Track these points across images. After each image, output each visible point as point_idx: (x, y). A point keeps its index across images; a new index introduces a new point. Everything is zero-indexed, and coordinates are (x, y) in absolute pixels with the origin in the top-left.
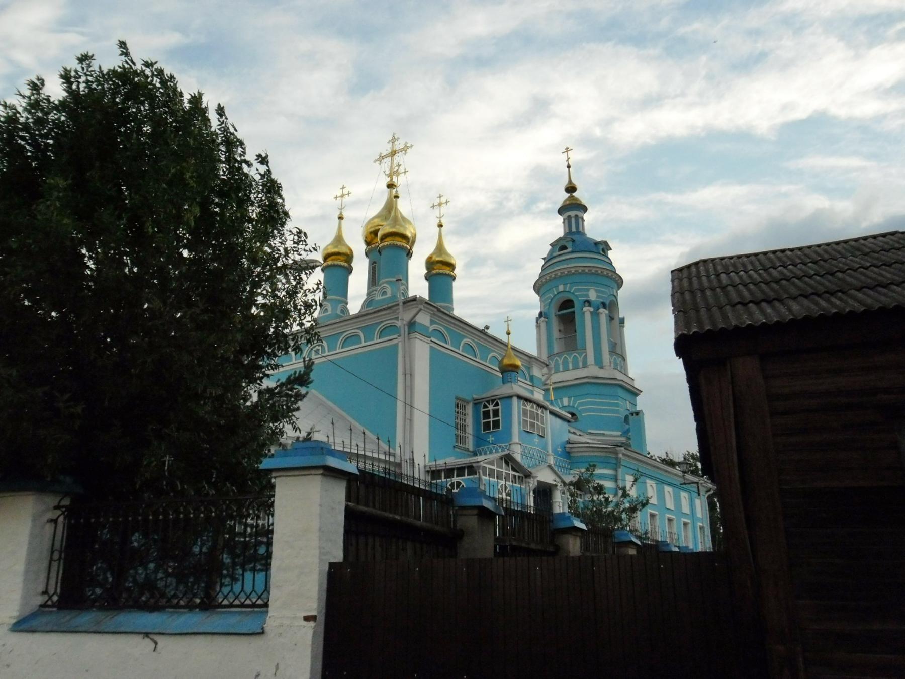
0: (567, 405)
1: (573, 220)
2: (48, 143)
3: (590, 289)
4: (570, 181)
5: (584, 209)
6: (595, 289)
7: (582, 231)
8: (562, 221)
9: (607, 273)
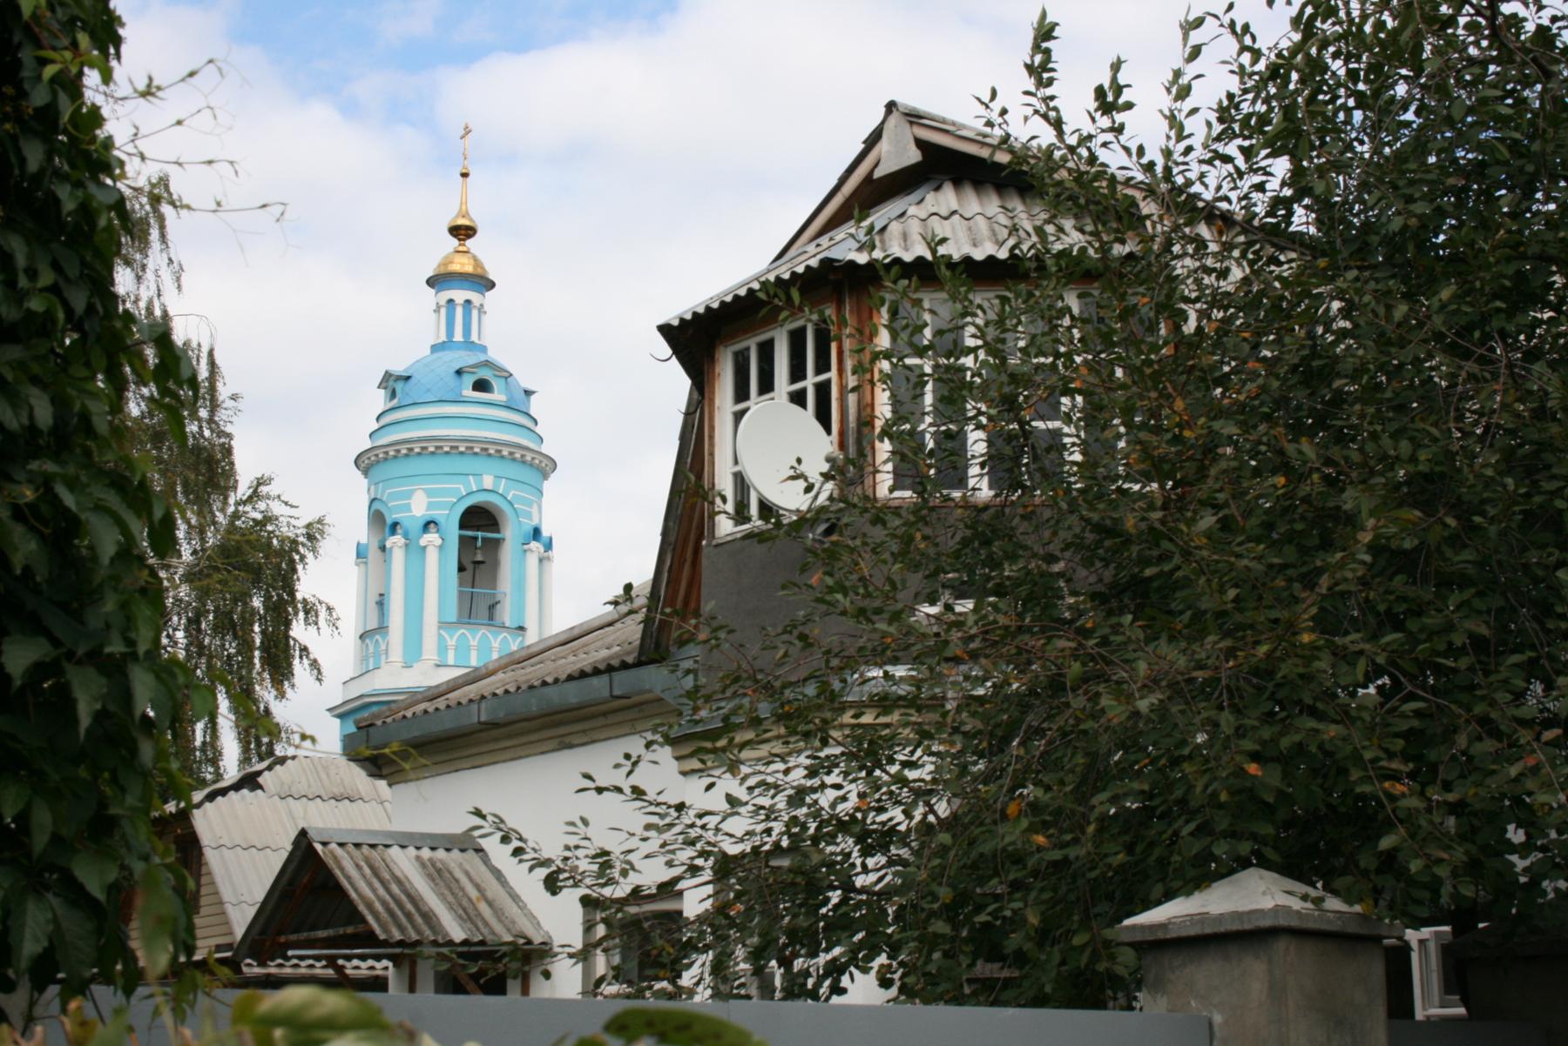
1: (459, 311)
9: (511, 453)
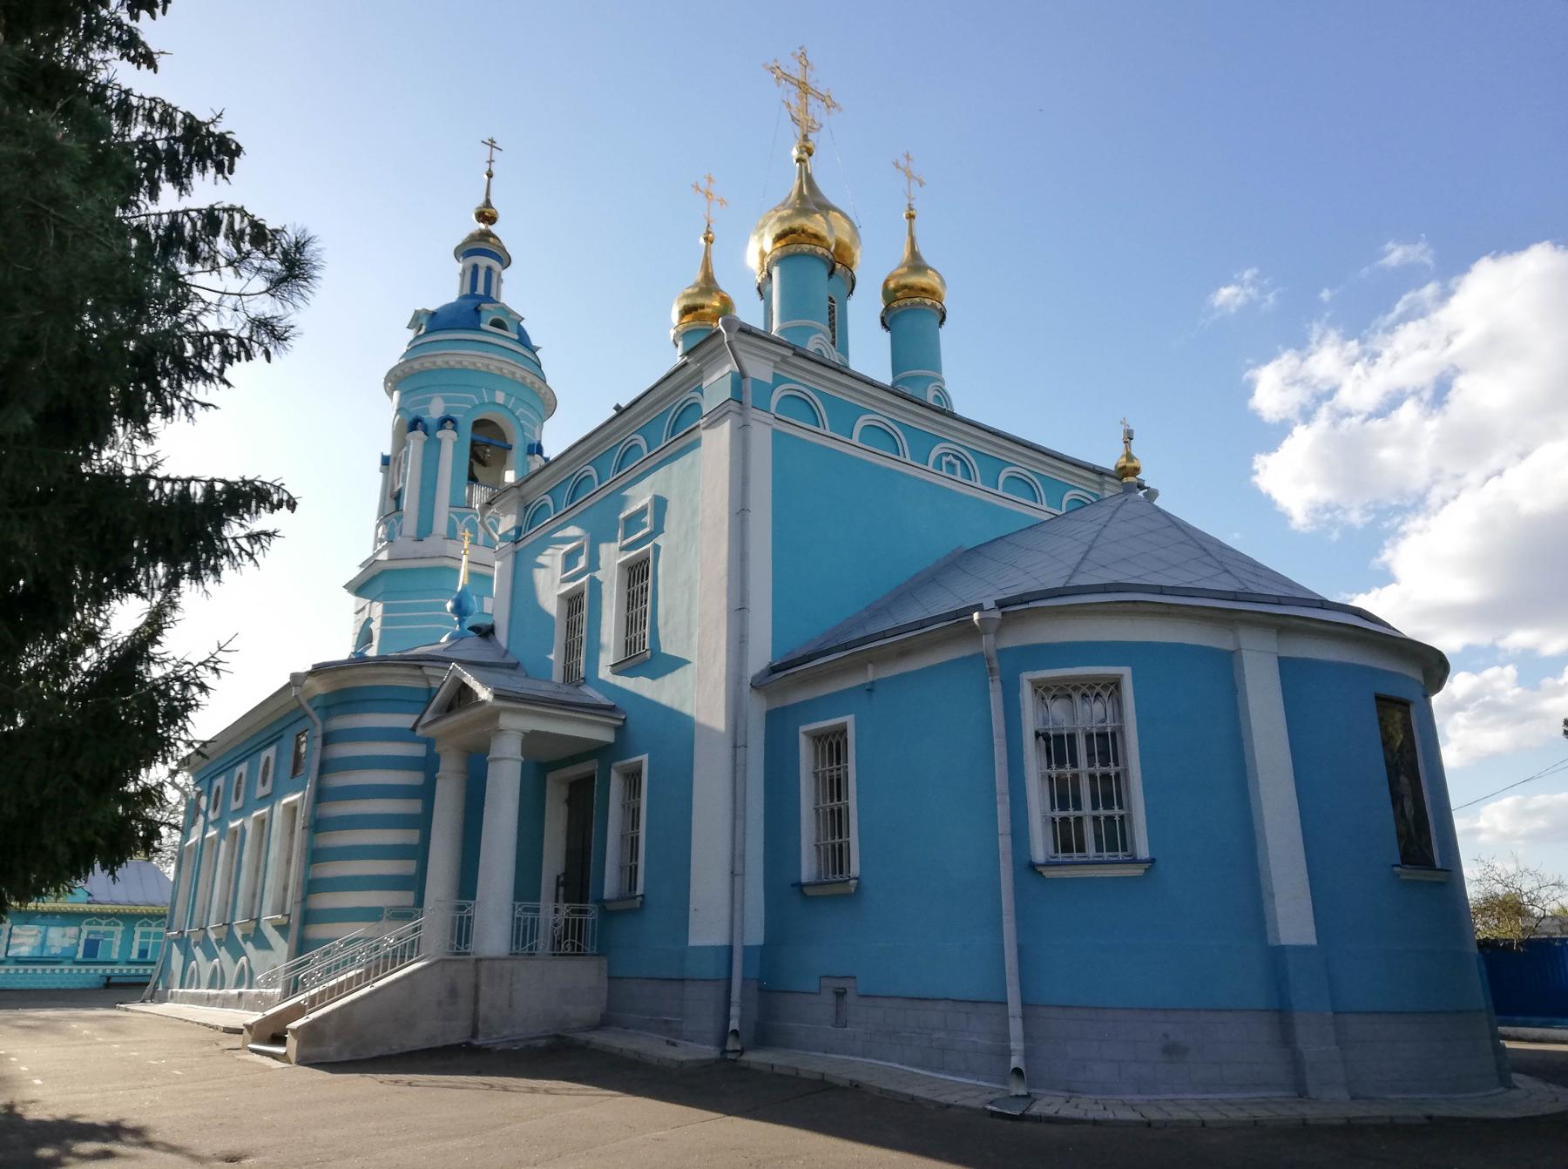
0: (501, 402)
2: (216, 150)
3: (431, 399)
4: (488, 203)
5: (505, 261)
6: (442, 397)
7: (495, 298)
8: (460, 270)
